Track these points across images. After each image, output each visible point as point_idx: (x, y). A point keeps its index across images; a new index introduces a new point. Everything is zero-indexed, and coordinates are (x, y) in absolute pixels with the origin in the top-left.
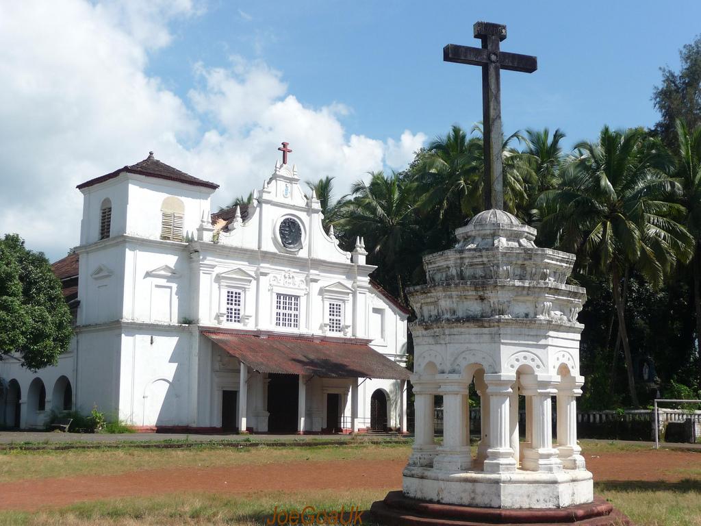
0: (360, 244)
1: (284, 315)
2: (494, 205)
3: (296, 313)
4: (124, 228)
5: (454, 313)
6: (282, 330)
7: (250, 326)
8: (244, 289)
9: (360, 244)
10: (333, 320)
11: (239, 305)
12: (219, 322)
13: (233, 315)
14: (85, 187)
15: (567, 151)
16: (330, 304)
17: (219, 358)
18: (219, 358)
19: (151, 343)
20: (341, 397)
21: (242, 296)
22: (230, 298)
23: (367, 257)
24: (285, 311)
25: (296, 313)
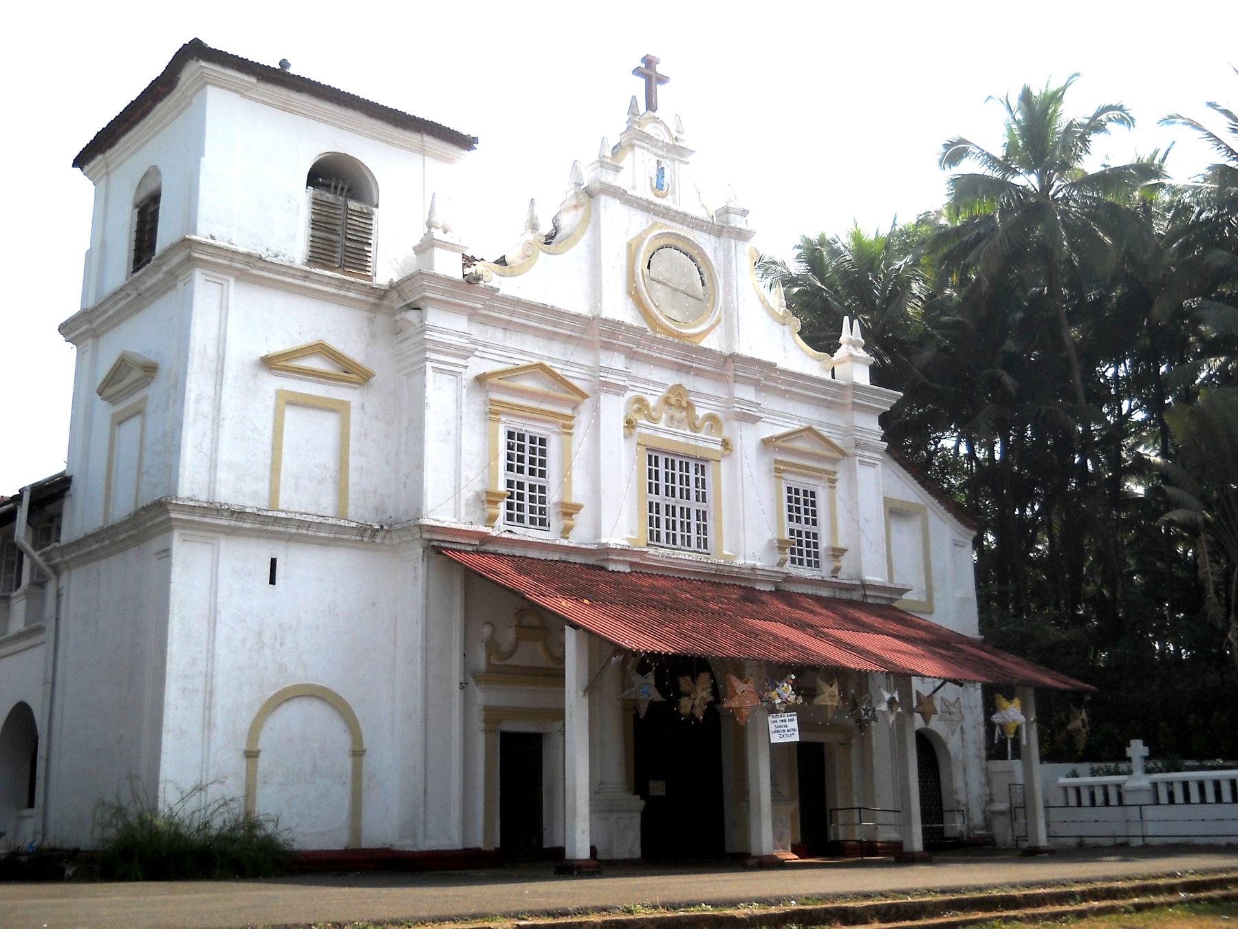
0: (851, 334)
1: (671, 510)
2: (80, 346)
3: (655, 499)
4: (190, 220)
5: (212, 361)
6: (661, 553)
7: (580, 536)
8: (567, 427)
9: (851, 334)
10: (799, 534)
11: (542, 474)
12: (491, 520)
13: (526, 503)
14: (92, 157)
15: (500, 292)
16: (789, 490)
17: (487, 631)
18: (487, 631)
19: (272, 581)
20: (125, 351)
21: (553, 448)
22: (537, 457)
23: (873, 369)
24: (671, 501)
25: (701, 506)
